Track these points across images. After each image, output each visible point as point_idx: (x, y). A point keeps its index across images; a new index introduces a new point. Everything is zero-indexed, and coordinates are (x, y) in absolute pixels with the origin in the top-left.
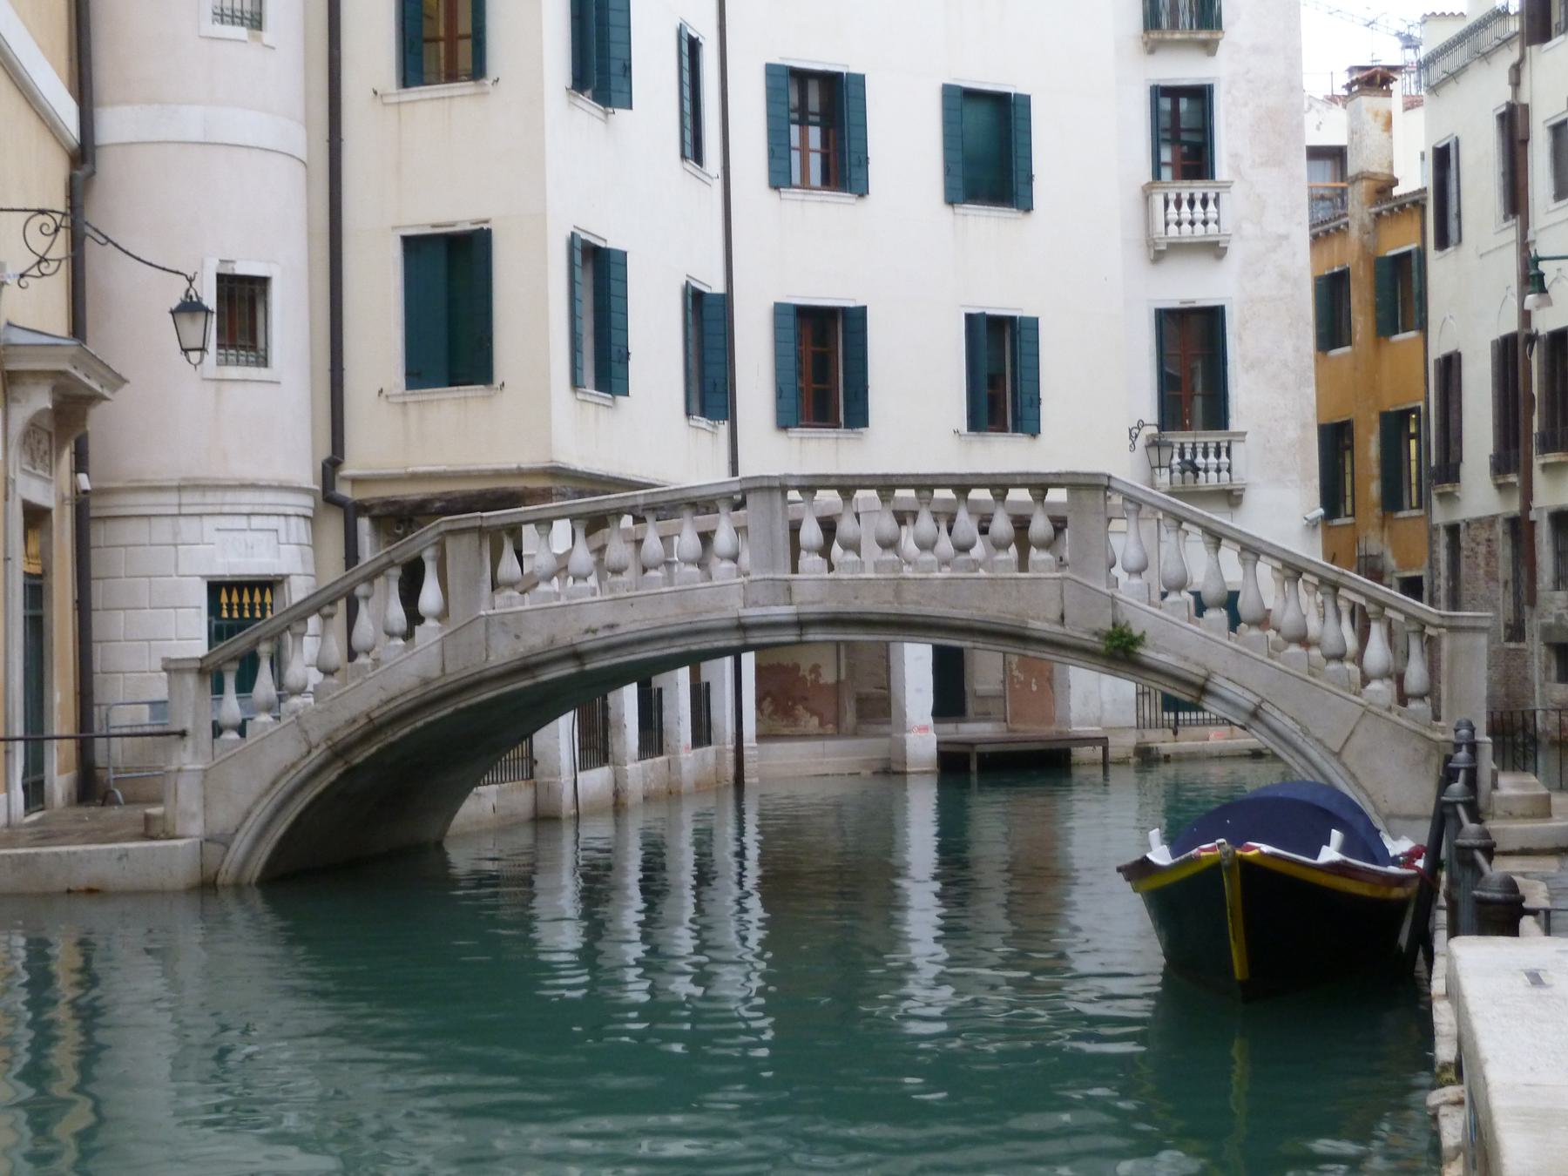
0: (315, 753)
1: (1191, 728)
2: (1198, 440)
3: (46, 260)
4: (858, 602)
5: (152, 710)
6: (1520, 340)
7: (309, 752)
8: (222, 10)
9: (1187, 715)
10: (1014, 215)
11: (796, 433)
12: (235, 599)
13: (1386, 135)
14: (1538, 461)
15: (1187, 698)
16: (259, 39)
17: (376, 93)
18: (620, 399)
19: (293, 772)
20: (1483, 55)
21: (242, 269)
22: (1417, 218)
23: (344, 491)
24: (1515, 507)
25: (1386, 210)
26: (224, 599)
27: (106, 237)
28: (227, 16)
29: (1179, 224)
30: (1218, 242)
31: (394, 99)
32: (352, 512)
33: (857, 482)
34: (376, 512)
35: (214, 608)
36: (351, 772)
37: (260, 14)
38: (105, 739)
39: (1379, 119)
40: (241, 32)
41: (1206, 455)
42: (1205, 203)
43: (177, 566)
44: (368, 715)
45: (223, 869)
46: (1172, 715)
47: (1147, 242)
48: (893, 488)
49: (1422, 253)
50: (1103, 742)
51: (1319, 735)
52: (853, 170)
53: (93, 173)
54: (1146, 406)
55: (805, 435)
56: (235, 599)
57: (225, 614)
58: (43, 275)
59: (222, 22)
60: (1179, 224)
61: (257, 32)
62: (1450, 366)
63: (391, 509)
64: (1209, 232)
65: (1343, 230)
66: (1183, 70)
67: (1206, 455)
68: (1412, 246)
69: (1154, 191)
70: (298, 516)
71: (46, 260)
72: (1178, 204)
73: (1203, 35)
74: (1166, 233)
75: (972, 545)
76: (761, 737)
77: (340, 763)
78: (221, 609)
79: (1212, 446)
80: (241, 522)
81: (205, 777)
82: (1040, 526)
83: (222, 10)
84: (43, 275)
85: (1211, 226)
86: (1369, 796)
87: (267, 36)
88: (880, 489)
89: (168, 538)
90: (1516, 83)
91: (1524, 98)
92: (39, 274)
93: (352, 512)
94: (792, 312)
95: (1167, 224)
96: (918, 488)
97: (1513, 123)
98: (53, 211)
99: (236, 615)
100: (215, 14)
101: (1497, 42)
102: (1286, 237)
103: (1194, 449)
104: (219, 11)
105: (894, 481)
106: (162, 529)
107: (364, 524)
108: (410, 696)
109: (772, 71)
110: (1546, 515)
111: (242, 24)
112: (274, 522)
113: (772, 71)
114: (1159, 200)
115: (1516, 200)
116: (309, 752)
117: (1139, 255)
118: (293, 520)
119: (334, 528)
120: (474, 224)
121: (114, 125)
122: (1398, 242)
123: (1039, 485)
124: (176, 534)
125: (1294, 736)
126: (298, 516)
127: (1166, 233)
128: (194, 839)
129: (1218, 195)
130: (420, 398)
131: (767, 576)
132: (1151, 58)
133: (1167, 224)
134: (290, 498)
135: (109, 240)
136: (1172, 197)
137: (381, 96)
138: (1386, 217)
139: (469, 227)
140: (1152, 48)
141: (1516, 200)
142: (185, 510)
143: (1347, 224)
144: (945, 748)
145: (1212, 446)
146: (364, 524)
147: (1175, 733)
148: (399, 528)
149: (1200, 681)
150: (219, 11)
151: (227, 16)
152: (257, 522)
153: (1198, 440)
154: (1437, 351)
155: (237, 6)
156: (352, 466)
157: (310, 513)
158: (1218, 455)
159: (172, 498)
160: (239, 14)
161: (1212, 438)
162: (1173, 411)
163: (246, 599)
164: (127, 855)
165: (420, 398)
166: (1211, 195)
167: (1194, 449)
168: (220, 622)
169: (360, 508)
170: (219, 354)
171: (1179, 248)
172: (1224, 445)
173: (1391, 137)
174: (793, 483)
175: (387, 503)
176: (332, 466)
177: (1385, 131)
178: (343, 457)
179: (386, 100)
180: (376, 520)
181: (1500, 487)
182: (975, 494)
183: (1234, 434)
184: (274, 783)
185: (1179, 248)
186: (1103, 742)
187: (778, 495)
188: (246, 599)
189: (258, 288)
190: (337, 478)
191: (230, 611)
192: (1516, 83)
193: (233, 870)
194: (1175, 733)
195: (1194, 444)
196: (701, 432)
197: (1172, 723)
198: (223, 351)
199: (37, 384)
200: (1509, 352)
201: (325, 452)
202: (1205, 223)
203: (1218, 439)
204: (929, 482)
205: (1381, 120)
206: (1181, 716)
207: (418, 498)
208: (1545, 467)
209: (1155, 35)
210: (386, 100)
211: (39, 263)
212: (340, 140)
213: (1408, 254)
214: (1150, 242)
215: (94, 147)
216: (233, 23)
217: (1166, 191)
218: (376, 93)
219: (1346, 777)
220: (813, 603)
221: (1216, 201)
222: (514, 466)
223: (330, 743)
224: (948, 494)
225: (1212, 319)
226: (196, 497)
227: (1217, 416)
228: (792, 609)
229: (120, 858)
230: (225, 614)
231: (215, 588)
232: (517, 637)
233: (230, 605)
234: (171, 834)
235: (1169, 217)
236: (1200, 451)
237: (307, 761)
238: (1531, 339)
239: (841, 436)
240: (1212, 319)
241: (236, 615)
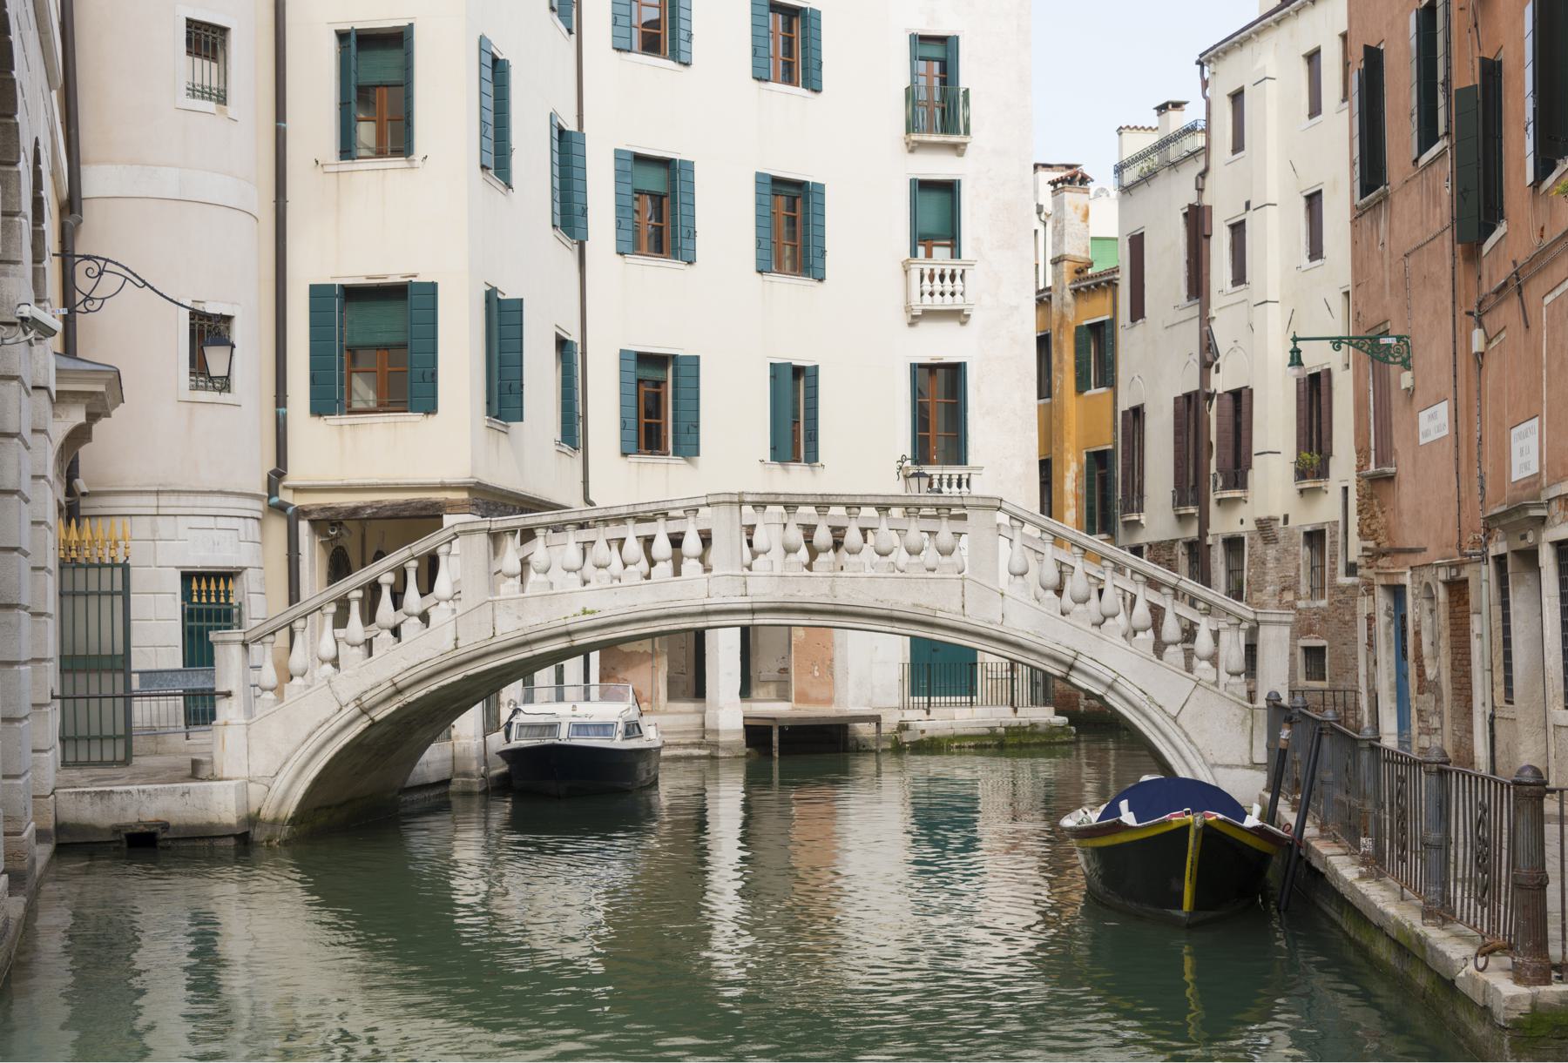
0: (345, 710)
1: (940, 709)
2: (945, 472)
3: (91, 299)
4: (799, 594)
5: (141, 679)
6: (1201, 397)
7: (340, 710)
8: (194, 86)
9: (938, 699)
10: (809, 283)
11: (634, 459)
12: (204, 586)
13: (1083, 225)
14: (1213, 498)
15: (1058, 673)
16: (222, 112)
17: (317, 162)
18: (514, 425)
19: (326, 726)
20: (1173, 164)
21: (211, 308)
22: (1109, 294)
23: (286, 496)
24: (1193, 532)
25: (1084, 287)
26: (195, 586)
27: (143, 281)
28: (198, 91)
29: (932, 294)
30: (963, 310)
31: (335, 169)
32: (293, 517)
33: (801, 499)
34: (314, 516)
35: (187, 594)
36: (374, 724)
37: (225, 91)
38: (85, 700)
39: (1078, 211)
40: (211, 106)
41: (950, 485)
42: (953, 278)
43: (155, 558)
44: (391, 679)
45: (265, 807)
46: (926, 699)
47: (905, 308)
48: (828, 505)
49: (1112, 322)
50: (876, 720)
51: (1160, 703)
52: (684, 240)
53: (81, 221)
54: (902, 442)
55: (643, 460)
56: (204, 586)
57: (195, 599)
58: (89, 311)
59: (194, 96)
60: (932, 294)
61: (223, 107)
62: (1137, 414)
63: (328, 514)
64: (946, 303)
65: (1045, 302)
66: (937, 167)
67: (950, 485)
68: (1107, 317)
69: (912, 266)
70: (253, 518)
71: (91, 299)
72: (932, 278)
73: (954, 139)
74: (921, 301)
75: (796, 551)
76: (784, 696)
77: (366, 718)
78: (192, 596)
79: (955, 478)
80: (210, 522)
81: (248, 729)
82: (823, 537)
83: (194, 86)
84: (89, 311)
85: (958, 296)
86: (1198, 750)
87: (231, 109)
88: (817, 506)
89: (148, 535)
90: (1200, 190)
91: (1206, 201)
92: (85, 310)
93: (293, 517)
94: (633, 357)
95: (922, 294)
96: (848, 506)
97: (1197, 219)
98: (97, 258)
99: (213, 600)
100: (188, 89)
101: (1186, 154)
102: (1017, 308)
103: (940, 480)
104: (191, 87)
105: (831, 500)
106: (141, 527)
107: (304, 526)
108: (427, 665)
109: (619, 155)
110: (1220, 541)
111: (211, 99)
112: (235, 523)
113: (619, 155)
114: (916, 275)
115: (1197, 285)
116: (340, 710)
117: (904, 318)
118: (250, 521)
119: (278, 528)
120: (368, 278)
121: (95, 181)
122: (1096, 311)
123: (823, 505)
124: (154, 531)
125: (1143, 704)
126: (253, 518)
127: (921, 301)
128: (238, 782)
129: (963, 271)
130: (355, 421)
131: (726, 573)
132: (911, 156)
133: (922, 294)
134: (249, 503)
135: (146, 284)
136: (927, 272)
137: (322, 166)
138: (1083, 292)
139: (399, 280)
140: (914, 148)
141: (1197, 285)
142: (162, 511)
143: (1050, 297)
144: (749, 722)
145: (945, 478)
146: (304, 526)
147: (928, 713)
148: (333, 530)
149: (1069, 660)
150: (191, 87)
151: (198, 91)
152: (222, 522)
153: (945, 472)
154: (1125, 404)
155: (206, 83)
156: (297, 473)
157: (259, 515)
158: (959, 485)
159: (151, 500)
160: (208, 90)
161: (955, 471)
162: (921, 452)
163: (213, 587)
164: (188, 793)
165: (355, 421)
166: (958, 272)
167: (940, 480)
168: (192, 606)
169: (301, 513)
170: (191, 380)
171: (930, 315)
172: (965, 477)
173: (1088, 226)
174: (749, 498)
175: (324, 509)
176: (277, 476)
177: (1083, 221)
178: (286, 470)
179: (327, 169)
180: (312, 522)
181: (1180, 517)
182: (833, 510)
183: (973, 468)
184: (310, 735)
185: (930, 315)
186: (876, 720)
187: (736, 508)
188: (213, 587)
189: (222, 326)
190: (280, 487)
191: (200, 597)
192: (1200, 190)
193: (273, 805)
194: (928, 713)
195: (941, 475)
196: (564, 455)
197: (926, 705)
198: (194, 378)
199: (76, 402)
200: (1190, 407)
201: (271, 465)
202: (953, 294)
203: (960, 472)
204: (858, 500)
205: (1080, 213)
206: (932, 699)
207: (352, 505)
208: (1219, 501)
209: (915, 137)
210: (327, 169)
211: (85, 301)
212: (286, 201)
213: (1103, 323)
214: (908, 308)
215: (81, 199)
216: (203, 98)
217: (922, 266)
218: (317, 162)
219: (1183, 736)
220: (764, 595)
221: (962, 277)
222: (438, 481)
223: (358, 702)
224: (842, 511)
225: (954, 374)
226: (173, 500)
227: (957, 452)
228: (748, 599)
229: (183, 794)
230: (195, 599)
231: (187, 577)
232: (519, 618)
233: (200, 593)
234: (219, 776)
235: (924, 288)
236: (955, 482)
237: (338, 717)
238: (1210, 397)
239: (671, 461)
240: (954, 374)
241: (213, 600)
